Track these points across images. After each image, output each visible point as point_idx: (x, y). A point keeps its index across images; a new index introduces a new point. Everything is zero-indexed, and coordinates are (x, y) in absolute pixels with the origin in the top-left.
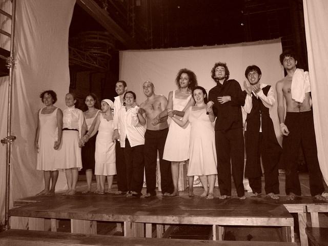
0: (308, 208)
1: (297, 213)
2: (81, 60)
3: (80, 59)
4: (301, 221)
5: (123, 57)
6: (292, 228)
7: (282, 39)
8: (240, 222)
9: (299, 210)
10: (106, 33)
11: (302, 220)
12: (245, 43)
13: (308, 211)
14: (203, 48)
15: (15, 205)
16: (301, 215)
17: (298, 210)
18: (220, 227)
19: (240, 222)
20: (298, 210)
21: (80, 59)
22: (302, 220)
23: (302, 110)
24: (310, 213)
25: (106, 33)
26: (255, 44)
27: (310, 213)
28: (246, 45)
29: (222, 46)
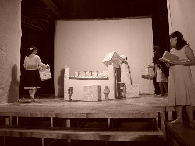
0: (166, 109)
1: (160, 112)
2: (30, 25)
3: (30, 24)
4: (162, 117)
5: (57, 25)
6: (157, 119)
7: (152, 15)
8: (125, 116)
9: (161, 110)
10: (47, 8)
11: (162, 116)
12: (130, 17)
13: (166, 111)
14: (106, 20)
15: (180, 110)
16: (162, 113)
17: (160, 110)
18: (30, 90)
19: (125, 116)
20: (160, 110)
21: (30, 24)
22: (162, 116)
23: (33, 137)
24: (167, 112)
25: (47, 8)
26: (136, 18)
27: (167, 112)
28: (130, 19)
29: (116, 19)
